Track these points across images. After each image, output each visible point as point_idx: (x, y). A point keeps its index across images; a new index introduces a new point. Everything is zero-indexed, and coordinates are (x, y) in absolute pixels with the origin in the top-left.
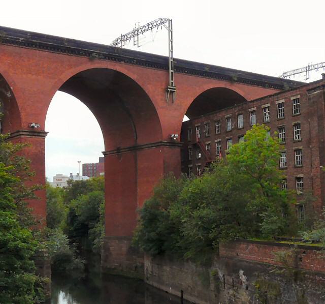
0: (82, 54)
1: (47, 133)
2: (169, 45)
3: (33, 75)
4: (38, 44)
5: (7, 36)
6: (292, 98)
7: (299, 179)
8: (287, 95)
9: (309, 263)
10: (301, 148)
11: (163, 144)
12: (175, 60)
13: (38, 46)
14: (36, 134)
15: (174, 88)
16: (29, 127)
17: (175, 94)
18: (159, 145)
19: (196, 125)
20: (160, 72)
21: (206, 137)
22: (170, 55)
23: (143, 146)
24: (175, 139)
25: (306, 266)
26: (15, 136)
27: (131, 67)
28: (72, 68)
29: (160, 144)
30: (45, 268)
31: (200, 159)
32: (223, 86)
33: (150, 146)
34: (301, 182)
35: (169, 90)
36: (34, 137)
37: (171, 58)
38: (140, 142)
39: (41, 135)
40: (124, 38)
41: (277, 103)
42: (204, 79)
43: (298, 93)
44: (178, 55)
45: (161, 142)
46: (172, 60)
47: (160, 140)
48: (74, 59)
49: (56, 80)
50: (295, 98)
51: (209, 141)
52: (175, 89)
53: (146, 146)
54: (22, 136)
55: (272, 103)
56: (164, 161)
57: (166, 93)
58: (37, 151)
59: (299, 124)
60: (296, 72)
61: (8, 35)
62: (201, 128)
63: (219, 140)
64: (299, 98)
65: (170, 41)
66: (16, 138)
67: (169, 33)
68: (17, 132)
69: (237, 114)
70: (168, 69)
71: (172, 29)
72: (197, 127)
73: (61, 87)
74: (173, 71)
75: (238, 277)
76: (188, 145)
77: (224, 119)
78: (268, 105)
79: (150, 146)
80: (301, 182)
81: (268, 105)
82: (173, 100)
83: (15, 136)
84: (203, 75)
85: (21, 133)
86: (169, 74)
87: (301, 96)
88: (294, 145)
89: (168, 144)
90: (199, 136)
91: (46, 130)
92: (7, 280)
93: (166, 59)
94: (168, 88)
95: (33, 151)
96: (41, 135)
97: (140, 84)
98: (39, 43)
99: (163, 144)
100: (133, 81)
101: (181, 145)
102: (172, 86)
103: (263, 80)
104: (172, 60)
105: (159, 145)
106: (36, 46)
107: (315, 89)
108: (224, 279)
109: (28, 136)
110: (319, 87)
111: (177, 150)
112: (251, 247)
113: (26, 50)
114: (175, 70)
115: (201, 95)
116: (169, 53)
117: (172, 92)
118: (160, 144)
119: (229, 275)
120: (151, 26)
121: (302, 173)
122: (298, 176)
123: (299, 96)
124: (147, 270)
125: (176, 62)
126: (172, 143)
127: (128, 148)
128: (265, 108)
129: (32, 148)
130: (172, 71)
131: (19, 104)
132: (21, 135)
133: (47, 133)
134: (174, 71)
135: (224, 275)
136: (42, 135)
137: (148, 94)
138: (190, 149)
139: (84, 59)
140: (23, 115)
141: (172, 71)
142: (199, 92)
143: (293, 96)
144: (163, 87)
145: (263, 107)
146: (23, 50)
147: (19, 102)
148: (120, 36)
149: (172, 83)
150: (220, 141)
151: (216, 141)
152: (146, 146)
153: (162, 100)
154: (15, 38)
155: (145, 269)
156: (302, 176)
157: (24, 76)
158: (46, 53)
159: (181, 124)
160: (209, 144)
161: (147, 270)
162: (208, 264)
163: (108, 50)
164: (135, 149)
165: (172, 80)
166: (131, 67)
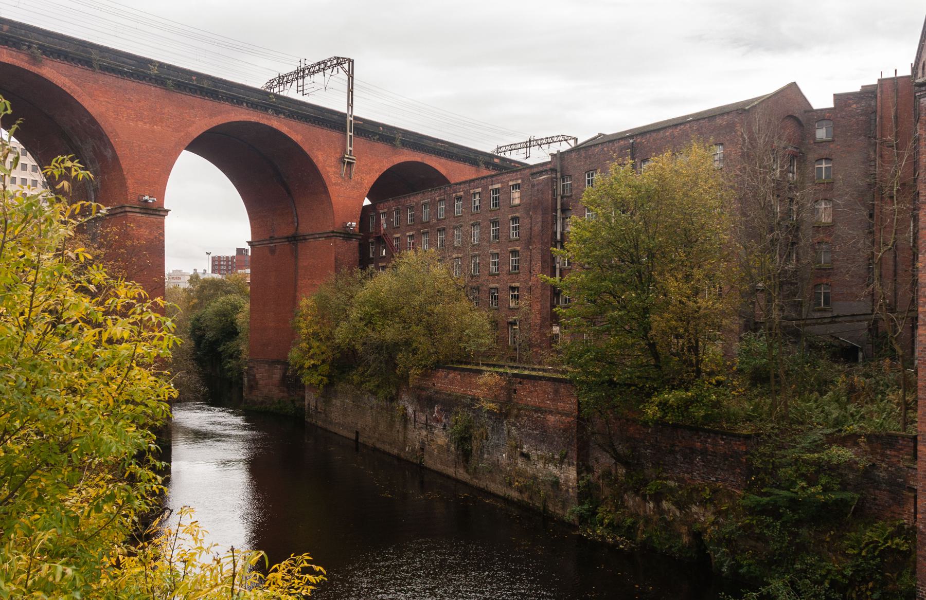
1: (167, 211)
3: (145, 123)
6: (511, 183)
7: (513, 289)
8: (506, 177)
9: (525, 396)
10: (518, 248)
12: (356, 118)
13: (153, 81)
14: (151, 212)
17: (354, 167)
19: (381, 211)
20: (335, 134)
21: (394, 228)
25: (522, 400)
31: (384, 257)
32: (419, 160)
34: (516, 293)
35: (346, 160)
37: (351, 116)
38: (305, 228)
41: (490, 187)
43: (519, 176)
46: (352, 119)
47: (331, 229)
49: (182, 134)
50: (514, 183)
51: (397, 233)
54: (128, 214)
55: (485, 188)
59: (518, 218)
60: (513, 147)
62: (388, 215)
63: (411, 233)
64: (519, 184)
68: (121, 207)
69: (437, 199)
70: (345, 131)
74: (352, 134)
76: (369, 238)
78: (479, 190)
80: (516, 293)
81: (479, 190)
82: (350, 174)
85: (128, 209)
87: (523, 181)
88: (510, 245)
90: (385, 226)
91: (166, 207)
93: (344, 116)
94: (344, 157)
97: (306, 148)
100: (295, 144)
102: (350, 155)
104: (352, 119)
107: (541, 173)
109: (138, 215)
110: (546, 171)
111: (354, 243)
112: (451, 375)
113: (134, 84)
117: (350, 164)
121: (518, 281)
122: (513, 285)
123: (519, 181)
124: (309, 405)
126: (347, 235)
127: (285, 238)
128: (475, 194)
131: (123, 167)
133: (167, 211)
135: (414, 411)
138: (372, 243)
140: (130, 182)
142: (386, 165)
143: (513, 180)
144: (338, 156)
145: (472, 191)
150: (413, 235)
151: (408, 234)
153: (335, 173)
155: (306, 403)
156: (517, 285)
160: (397, 238)
161: (309, 405)
164: (295, 239)
165: (351, 146)
166: (293, 123)
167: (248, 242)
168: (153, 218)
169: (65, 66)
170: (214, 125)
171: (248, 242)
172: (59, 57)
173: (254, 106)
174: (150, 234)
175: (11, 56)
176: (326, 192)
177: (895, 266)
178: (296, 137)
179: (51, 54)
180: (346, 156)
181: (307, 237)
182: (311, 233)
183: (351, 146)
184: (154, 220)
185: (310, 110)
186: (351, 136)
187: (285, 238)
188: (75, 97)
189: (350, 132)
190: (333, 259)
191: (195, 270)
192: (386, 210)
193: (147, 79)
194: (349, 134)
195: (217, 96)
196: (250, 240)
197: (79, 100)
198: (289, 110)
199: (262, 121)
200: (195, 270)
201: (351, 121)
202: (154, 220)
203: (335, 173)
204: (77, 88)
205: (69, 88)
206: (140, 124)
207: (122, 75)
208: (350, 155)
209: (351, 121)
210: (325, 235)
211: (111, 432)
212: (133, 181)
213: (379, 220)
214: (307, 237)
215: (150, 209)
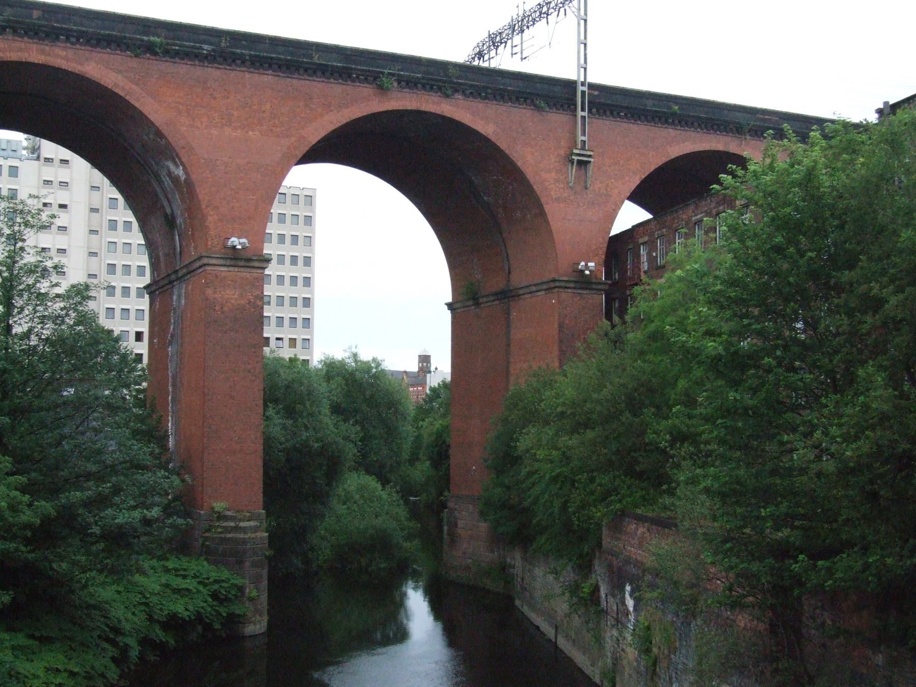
0: (471, 93)
2: (579, 52)
4: (247, 58)
5: (170, 41)
11: (557, 284)
12: (592, 86)
14: (242, 263)
15: (588, 153)
16: (225, 247)
17: (591, 167)
18: (552, 286)
19: (641, 241)
20: (557, 118)
22: (579, 75)
23: (522, 288)
24: (587, 272)
26: (197, 269)
27: (481, 106)
28: (332, 111)
29: (552, 285)
30: (247, 564)
32: (720, 147)
33: (534, 289)
35: (575, 158)
36: (236, 269)
38: (519, 279)
39: (251, 264)
40: (495, 41)
42: (671, 132)
44: (595, 77)
45: (554, 281)
46: (585, 89)
47: (553, 275)
48: (336, 89)
52: (590, 156)
53: (527, 290)
56: (561, 326)
57: (570, 165)
58: (242, 302)
61: (173, 39)
65: (580, 42)
66: (199, 271)
67: (579, 24)
70: (575, 110)
71: (586, 14)
72: (643, 244)
73: (632, 194)
74: (585, 114)
75: (623, 603)
77: (691, 225)
79: (534, 289)
82: (586, 182)
83: (197, 269)
84: (666, 122)
85: (205, 261)
86: (575, 123)
89: (572, 285)
92: (91, 599)
93: (570, 86)
94: (572, 154)
95: (233, 301)
96: (251, 264)
97: (503, 145)
98: (251, 56)
99: (557, 284)
100: (485, 139)
101: (606, 287)
102: (583, 148)
103: (740, 117)
104: (585, 89)
105: (552, 286)
106: (243, 62)
108: (607, 602)
113: (218, 73)
114: (594, 110)
115: (347, 125)
116: (579, 72)
117: (583, 164)
118: (552, 285)
119: (614, 596)
120: (545, 9)
125: (596, 93)
126: (583, 282)
127: (493, 295)
129: (230, 296)
130: (583, 114)
131: (201, 197)
132: (205, 265)
134: (590, 111)
135: (606, 596)
136: (256, 264)
137: (521, 168)
139: (366, 90)
141: (583, 114)
142: (655, 161)
144: (562, 152)
146: (214, 74)
147: (202, 193)
148: (487, 35)
149: (584, 142)
152: (527, 290)
154: (193, 47)
157: (215, 132)
158: (267, 79)
159: (607, 240)
162: (585, 567)
163: (423, 69)
164: (507, 295)
165: (584, 134)
167: (447, 304)
168: (246, 274)
169: (118, 59)
170: (345, 122)
171: (447, 304)
172: (109, 45)
173: (410, 84)
174: (241, 296)
175: (43, 52)
176: (542, 214)
177: (192, 271)
178: (486, 128)
179: (26, 33)
180: (575, 151)
181: (521, 292)
182: (526, 284)
183: (584, 134)
184: (248, 275)
185: (520, 83)
186: (583, 118)
187: (493, 295)
188: (133, 102)
189: (583, 110)
190: (556, 326)
191: (296, 355)
192: (646, 239)
193: (239, 62)
194: (580, 113)
195: (350, 76)
196: (450, 300)
197: (137, 105)
198: (472, 86)
199: (424, 108)
200: (296, 355)
201: (583, 92)
202: (248, 275)
203: (557, 181)
204: (134, 87)
205: (123, 89)
206: (227, 131)
207: (200, 61)
208: (583, 148)
209: (583, 92)
210: (545, 287)
211: (19, 676)
212: (216, 217)
213: (638, 255)
214: (521, 292)
215: (241, 259)
